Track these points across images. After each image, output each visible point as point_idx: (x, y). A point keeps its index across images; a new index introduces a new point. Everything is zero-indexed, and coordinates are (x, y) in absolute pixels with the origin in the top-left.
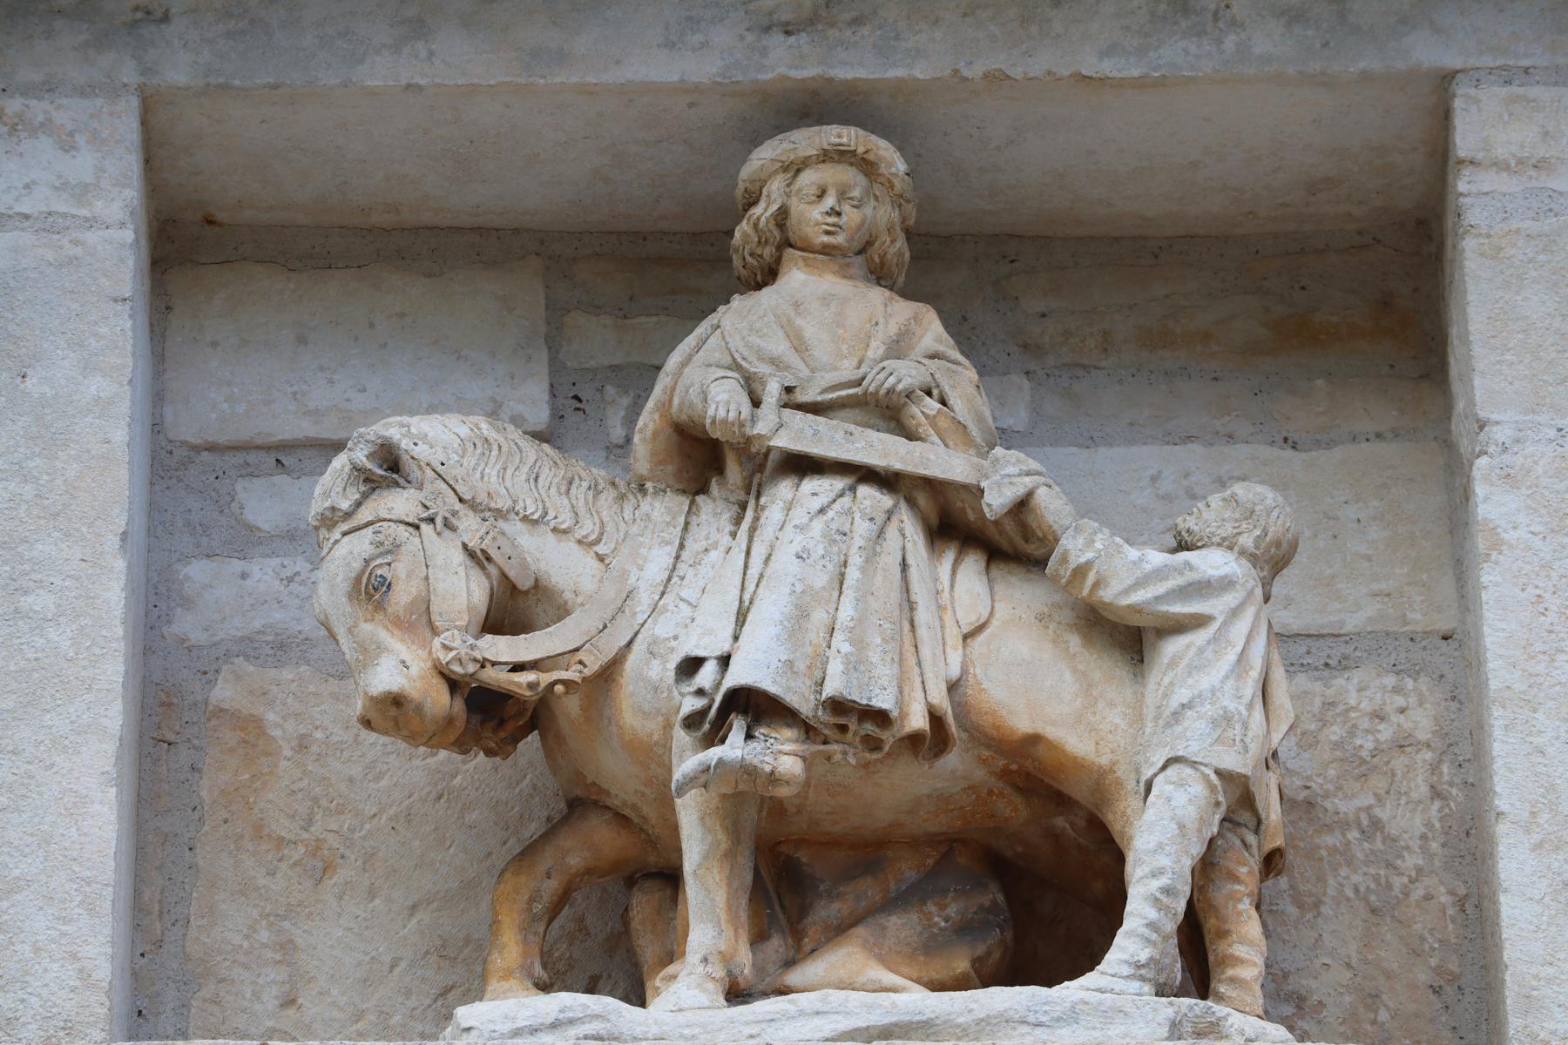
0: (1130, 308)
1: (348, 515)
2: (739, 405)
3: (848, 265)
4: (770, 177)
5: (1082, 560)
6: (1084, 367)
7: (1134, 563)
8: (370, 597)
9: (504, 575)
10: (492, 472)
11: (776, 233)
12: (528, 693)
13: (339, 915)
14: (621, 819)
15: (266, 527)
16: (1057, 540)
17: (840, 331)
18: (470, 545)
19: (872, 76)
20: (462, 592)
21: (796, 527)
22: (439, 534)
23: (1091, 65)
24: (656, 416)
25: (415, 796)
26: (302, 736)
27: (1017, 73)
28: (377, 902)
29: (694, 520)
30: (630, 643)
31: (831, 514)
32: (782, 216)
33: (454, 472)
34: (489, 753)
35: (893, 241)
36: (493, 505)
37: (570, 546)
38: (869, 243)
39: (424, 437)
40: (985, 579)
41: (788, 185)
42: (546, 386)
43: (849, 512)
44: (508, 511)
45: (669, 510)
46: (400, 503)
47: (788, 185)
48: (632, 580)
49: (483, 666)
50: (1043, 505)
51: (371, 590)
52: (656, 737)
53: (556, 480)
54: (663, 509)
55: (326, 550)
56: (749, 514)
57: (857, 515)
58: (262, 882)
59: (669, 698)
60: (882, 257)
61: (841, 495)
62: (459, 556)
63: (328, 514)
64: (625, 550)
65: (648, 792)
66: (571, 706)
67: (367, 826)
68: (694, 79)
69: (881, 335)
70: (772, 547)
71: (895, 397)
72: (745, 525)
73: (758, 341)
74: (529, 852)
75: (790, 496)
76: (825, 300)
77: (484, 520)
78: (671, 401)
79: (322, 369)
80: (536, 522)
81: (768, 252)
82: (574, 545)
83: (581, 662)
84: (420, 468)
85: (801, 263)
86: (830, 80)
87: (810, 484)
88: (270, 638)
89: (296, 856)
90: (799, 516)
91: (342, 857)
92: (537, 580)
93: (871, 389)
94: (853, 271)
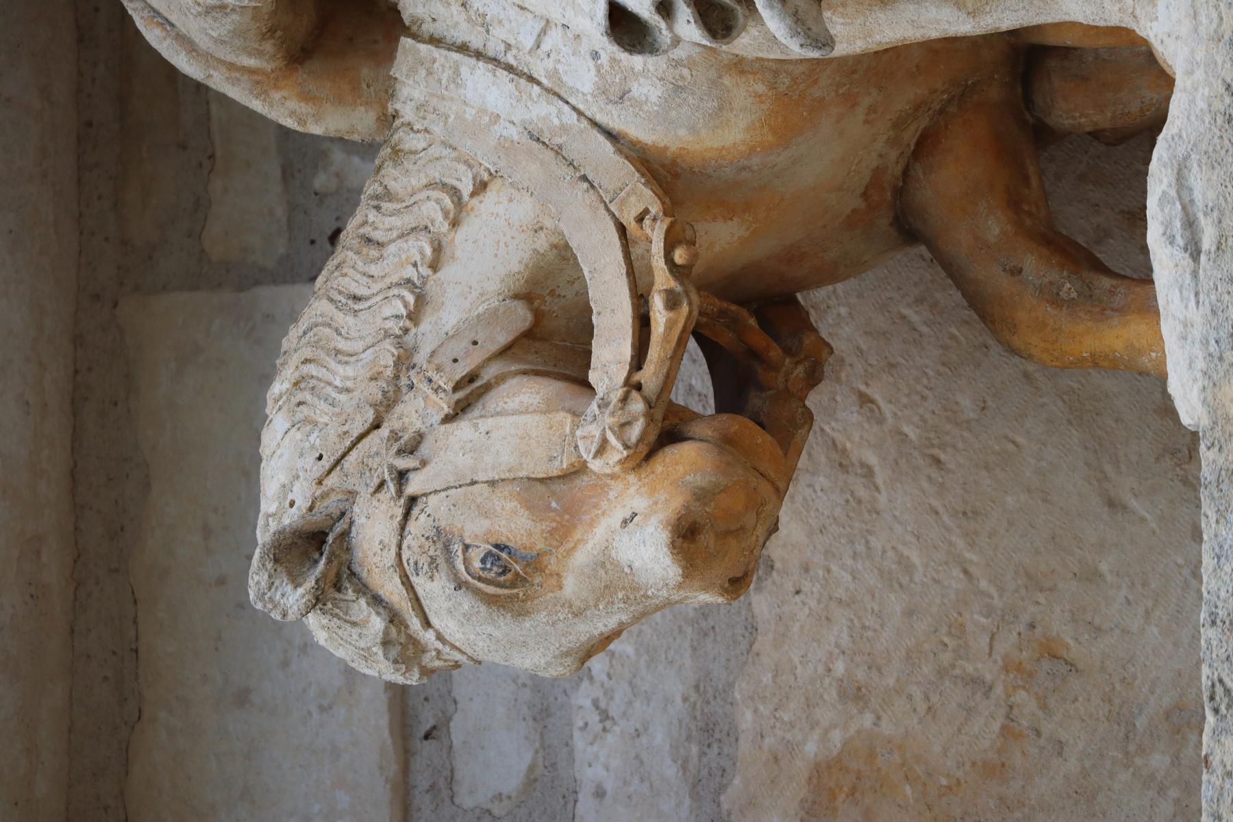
1: (394, 618)
8: (518, 581)
9: (505, 352)
10: (341, 373)
12: (685, 309)
13: (1125, 631)
14: (925, 146)
15: (528, 757)
18: (446, 410)
20: (523, 423)
22: (424, 463)
24: (276, 95)
25: (936, 503)
26: (843, 695)
28: (1104, 567)
29: (428, 28)
30: (611, 135)
33: (333, 438)
34: (814, 378)
36: (389, 372)
37: (461, 240)
39: (285, 488)
44: (400, 346)
46: (374, 528)
48: (513, 133)
49: (639, 387)
51: (508, 578)
52: (760, 88)
54: (416, 77)
55: (458, 656)
58: (1072, 765)
59: (690, 64)
62: (463, 430)
63: (394, 652)
64: (467, 146)
65: (866, 102)
66: (723, 238)
67: (984, 584)
74: (986, 310)
77: (411, 387)
78: (251, 71)
79: (285, 664)
80: (421, 299)
82: (461, 234)
83: (640, 219)
84: (325, 496)
88: (694, 749)
89: (1032, 705)
91: (1032, 626)
92: (516, 297)
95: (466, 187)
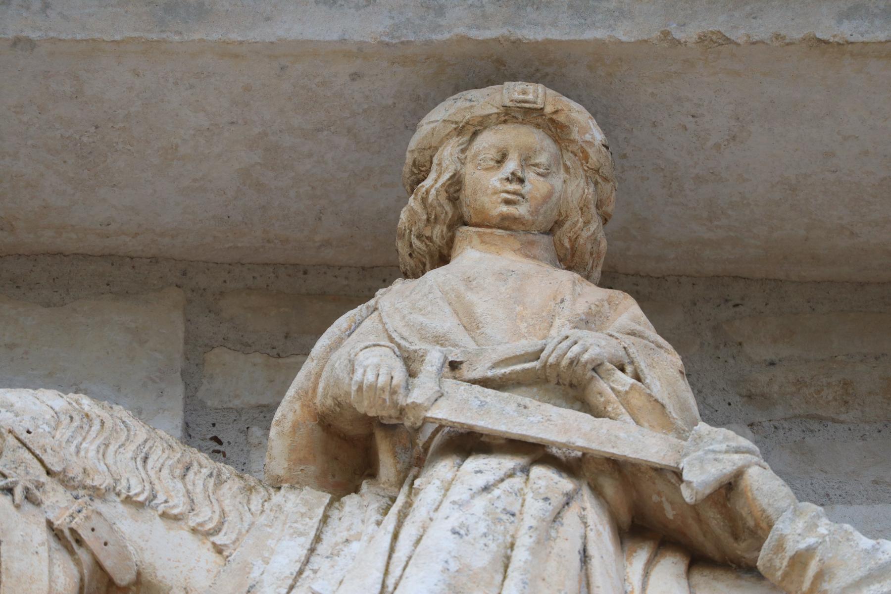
0: (876, 358)
2: (391, 369)
3: (531, 243)
4: (441, 142)
5: (802, 545)
6: (820, 419)
7: (867, 552)
9: (98, 565)
10: (90, 448)
11: (448, 208)
16: (770, 527)
17: (519, 309)
18: (57, 523)
19: (566, 38)
21: (454, 503)
22: (18, 507)
23: (828, 28)
24: (297, 406)
27: (738, 35)
29: (335, 514)
31: (496, 492)
32: (455, 185)
33: (42, 441)
35: (587, 223)
36: (89, 482)
38: (558, 223)
40: (684, 582)
41: (463, 151)
42: (179, 421)
43: (520, 493)
44: (108, 490)
45: (306, 502)
47: (463, 151)
48: (255, 574)
50: (755, 486)
53: (170, 462)
54: (302, 504)
56: (401, 499)
57: (529, 497)
60: (574, 241)
61: (511, 475)
62: (41, 535)
68: (357, 38)
69: (567, 312)
70: (425, 529)
71: (579, 370)
72: (395, 509)
73: (421, 319)
75: (449, 476)
76: (502, 276)
80: (141, 505)
81: (438, 232)
85: (476, 240)
86: (517, 43)
87: (473, 463)
90: (459, 492)
92: (139, 574)
93: (552, 360)
94: (537, 251)
95: (219, 539)
